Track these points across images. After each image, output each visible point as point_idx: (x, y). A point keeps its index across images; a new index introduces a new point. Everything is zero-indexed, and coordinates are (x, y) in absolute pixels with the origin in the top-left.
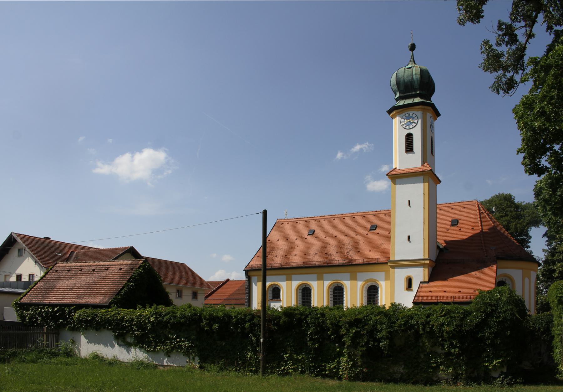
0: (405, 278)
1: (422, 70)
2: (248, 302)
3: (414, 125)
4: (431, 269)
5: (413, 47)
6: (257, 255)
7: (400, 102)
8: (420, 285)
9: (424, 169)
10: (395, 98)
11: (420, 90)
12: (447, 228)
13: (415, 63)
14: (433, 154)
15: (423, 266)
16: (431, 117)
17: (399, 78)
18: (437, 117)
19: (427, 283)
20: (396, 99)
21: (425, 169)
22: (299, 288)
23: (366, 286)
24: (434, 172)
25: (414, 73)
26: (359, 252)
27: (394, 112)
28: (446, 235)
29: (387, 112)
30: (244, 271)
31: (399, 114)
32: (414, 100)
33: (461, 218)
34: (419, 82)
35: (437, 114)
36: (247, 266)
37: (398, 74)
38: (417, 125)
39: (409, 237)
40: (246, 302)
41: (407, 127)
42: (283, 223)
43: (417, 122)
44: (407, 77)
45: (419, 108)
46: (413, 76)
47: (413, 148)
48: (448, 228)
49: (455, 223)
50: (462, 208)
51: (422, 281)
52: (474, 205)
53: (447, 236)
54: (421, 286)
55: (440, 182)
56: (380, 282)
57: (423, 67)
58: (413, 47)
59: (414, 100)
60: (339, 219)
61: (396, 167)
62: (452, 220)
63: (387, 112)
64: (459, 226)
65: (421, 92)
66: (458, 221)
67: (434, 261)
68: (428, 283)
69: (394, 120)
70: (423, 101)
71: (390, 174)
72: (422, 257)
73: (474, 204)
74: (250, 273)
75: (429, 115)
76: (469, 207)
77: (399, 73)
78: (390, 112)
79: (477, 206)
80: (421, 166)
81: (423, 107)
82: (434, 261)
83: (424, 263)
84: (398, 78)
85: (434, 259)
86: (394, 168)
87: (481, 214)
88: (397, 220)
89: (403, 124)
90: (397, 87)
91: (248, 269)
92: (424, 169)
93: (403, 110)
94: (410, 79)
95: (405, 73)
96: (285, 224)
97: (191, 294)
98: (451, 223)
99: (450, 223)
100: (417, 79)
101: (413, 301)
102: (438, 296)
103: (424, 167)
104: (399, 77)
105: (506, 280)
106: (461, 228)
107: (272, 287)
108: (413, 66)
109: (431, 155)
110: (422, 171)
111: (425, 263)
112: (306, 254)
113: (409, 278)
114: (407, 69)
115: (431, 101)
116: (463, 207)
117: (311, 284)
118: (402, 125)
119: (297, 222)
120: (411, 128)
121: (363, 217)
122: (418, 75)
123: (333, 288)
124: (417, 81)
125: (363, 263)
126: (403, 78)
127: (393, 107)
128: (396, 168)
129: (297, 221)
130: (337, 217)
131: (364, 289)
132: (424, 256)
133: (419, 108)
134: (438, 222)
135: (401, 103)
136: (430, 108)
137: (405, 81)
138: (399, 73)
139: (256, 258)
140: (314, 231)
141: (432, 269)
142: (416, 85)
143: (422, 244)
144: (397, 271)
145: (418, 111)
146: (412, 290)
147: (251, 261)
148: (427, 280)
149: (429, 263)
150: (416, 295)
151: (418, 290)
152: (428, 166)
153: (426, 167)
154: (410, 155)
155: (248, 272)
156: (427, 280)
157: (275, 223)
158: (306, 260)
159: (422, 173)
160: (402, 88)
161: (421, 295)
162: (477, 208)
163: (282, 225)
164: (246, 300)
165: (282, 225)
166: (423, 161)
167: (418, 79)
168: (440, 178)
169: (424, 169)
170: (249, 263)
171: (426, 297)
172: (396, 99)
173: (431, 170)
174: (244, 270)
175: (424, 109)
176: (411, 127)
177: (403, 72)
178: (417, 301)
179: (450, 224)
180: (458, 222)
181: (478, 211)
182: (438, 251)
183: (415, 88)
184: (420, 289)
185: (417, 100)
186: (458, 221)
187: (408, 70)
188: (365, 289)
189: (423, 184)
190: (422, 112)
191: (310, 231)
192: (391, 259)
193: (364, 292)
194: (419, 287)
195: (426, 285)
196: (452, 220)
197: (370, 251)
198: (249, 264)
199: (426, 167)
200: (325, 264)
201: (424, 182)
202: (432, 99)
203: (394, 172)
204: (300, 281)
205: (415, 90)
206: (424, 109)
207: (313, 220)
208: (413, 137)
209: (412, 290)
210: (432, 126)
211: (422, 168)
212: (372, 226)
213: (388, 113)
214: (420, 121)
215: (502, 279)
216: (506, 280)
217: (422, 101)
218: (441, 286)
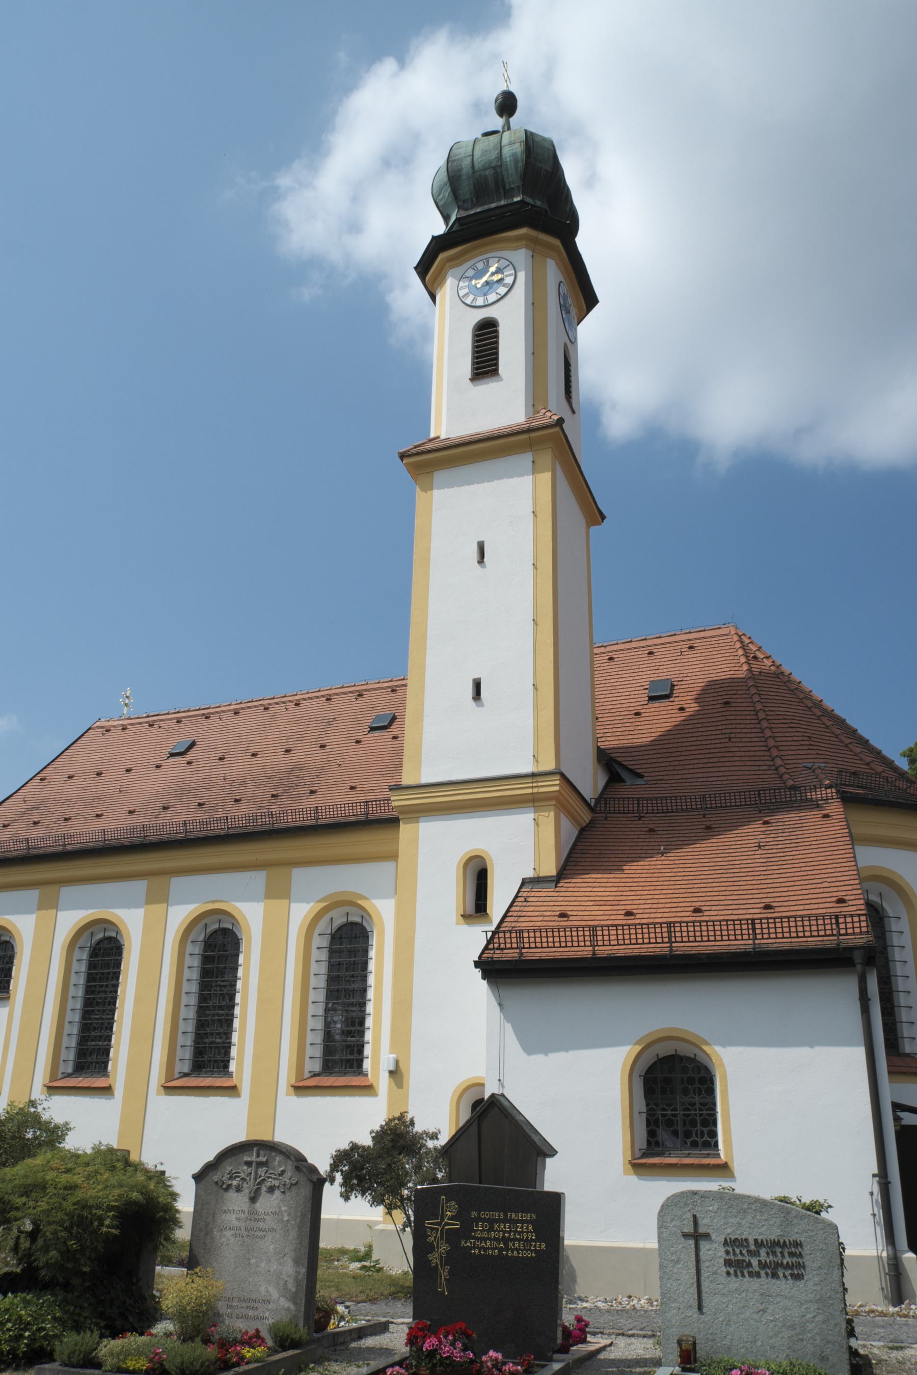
0: (458, 865)
3: (502, 290)
8: (519, 891)
11: (523, 193)
15: (533, 801)
16: (561, 282)
17: (458, 159)
19: (553, 884)
23: (323, 926)
26: (312, 792)
28: (631, 728)
34: (520, 164)
38: (513, 292)
39: (477, 685)
44: (482, 155)
45: (518, 239)
46: (501, 150)
47: (497, 364)
51: (530, 874)
52: (726, 637)
53: (636, 732)
54: (525, 894)
56: (374, 901)
61: (437, 435)
66: (673, 686)
68: (558, 882)
76: (708, 643)
83: (535, 790)
84: (454, 161)
86: (432, 435)
88: (431, 622)
89: (467, 294)
90: (449, 189)
94: (493, 158)
100: (514, 155)
101: (480, 957)
106: (685, 706)
111: (542, 790)
117: (122, 921)
118: (463, 296)
120: (490, 301)
122: (517, 145)
124: (516, 161)
125: (313, 822)
126: (469, 159)
132: (537, 761)
134: (598, 686)
137: (477, 167)
141: (576, 833)
142: (513, 177)
143: (529, 712)
145: (516, 248)
148: (550, 869)
149: (557, 788)
151: (508, 911)
154: (488, 387)
159: (526, 436)
160: (466, 189)
165: (103, 734)
166: (533, 405)
167: (519, 155)
176: (492, 298)
177: (472, 144)
178: (497, 955)
183: (507, 187)
184: (517, 909)
186: (673, 686)
189: (529, 479)
190: (530, 253)
192: (406, 780)
193: (316, 955)
194: (514, 901)
195: (548, 891)
201: (535, 471)
204: (87, 908)
208: (497, 332)
214: (521, 276)
218: (612, 894)
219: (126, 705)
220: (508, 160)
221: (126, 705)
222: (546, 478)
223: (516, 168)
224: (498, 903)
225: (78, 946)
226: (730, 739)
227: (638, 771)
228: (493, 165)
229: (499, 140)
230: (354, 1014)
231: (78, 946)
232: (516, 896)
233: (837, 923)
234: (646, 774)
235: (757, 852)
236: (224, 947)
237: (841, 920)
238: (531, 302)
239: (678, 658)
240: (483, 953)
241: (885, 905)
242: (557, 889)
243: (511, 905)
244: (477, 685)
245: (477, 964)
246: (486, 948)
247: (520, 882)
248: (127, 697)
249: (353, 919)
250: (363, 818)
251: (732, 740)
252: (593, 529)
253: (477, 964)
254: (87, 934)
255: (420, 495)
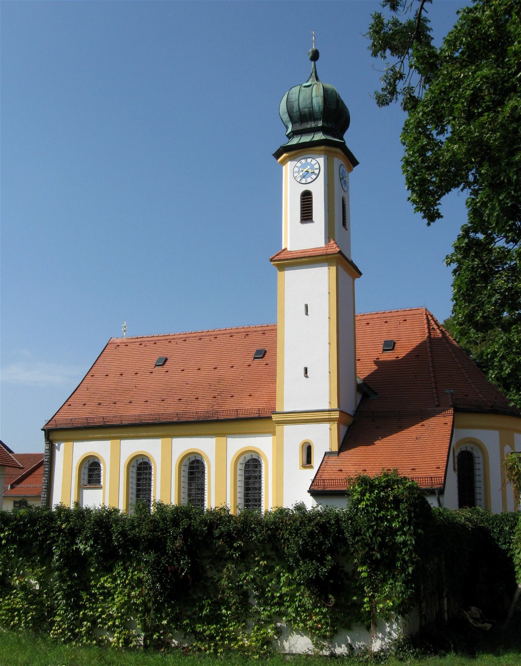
1: (325, 90)
2: (46, 490)
3: (314, 177)
4: (344, 429)
5: (315, 56)
6: (68, 403)
7: (293, 139)
8: (324, 458)
9: (328, 251)
10: (287, 134)
12: (377, 355)
13: (317, 79)
14: (347, 228)
18: (354, 167)
19: (337, 455)
20: (287, 136)
21: (330, 250)
22: (184, 463)
24: (346, 255)
25: (314, 94)
27: (285, 155)
29: (273, 155)
30: (43, 432)
31: (291, 158)
32: (313, 137)
33: (399, 337)
34: (321, 108)
35: (354, 162)
36: (50, 421)
37: (290, 96)
39: (306, 370)
40: (44, 490)
41: (303, 181)
42: (118, 346)
43: (318, 173)
45: (321, 151)
47: (312, 215)
48: (379, 355)
49: (391, 347)
50: (401, 321)
51: (328, 450)
55: (360, 274)
57: (329, 86)
58: (315, 56)
59: (313, 137)
60: (208, 338)
61: (286, 247)
62: (385, 342)
63: (273, 155)
64: (396, 351)
65: (325, 124)
67: (352, 414)
69: (284, 167)
70: (326, 139)
71: (277, 258)
72: (327, 407)
73: (420, 314)
74: (53, 436)
75: (337, 162)
77: (292, 94)
78: (277, 155)
79: (425, 317)
80: (324, 246)
81: (328, 148)
82: (352, 414)
84: (290, 102)
85: (351, 409)
86: (283, 248)
87: (431, 331)
91: (49, 427)
92: (328, 251)
93: (298, 153)
95: (300, 95)
96: (122, 348)
97: (477, 468)
98: (384, 347)
99: (381, 347)
101: (310, 489)
102: (432, 478)
103: (329, 248)
104: (291, 100)
105: (472, 448)
107: (89, 461)
108: (313, 84)
109: (343, 229)
110: (326, 255)
111: (332, 417)
112: (147, 401)
113: (248, 457)
114: (303, 89)
115: (343, 140)
116: (404, 319)
119: (141, 344)
121: (246, 335)
122: (320, 97)
123: (188, 463)
127: (281, 147)
128: (286, 249)
129: (141, 342)
130: (205, 336)
131: (239, 466)
133: (321, 151)
135: (295, 141)
136: (339, 150)
138: (292, 94)
139: (66, 407)
140: (166, 360)
144: (288, 429)
146: (312, 467)
147: (57, 413)
148: (336, 449)
149: (338, 416)
150: (315, 477)
151: (320, 468)
152: (335, 246)
153: (332, 248)
154: (308, 226)
155: (50, 434)
156: (337, 450)
157: (106, 346)
158: (147, 412)
159: (325, 257)
161: (323, 477)
162: (425, 321)
163: (116, 348)
164: (44, 487)
165: (116, 348)
168: (360, 268)
169: (330, 251)
170: (54, 416)
171: (435, 479)
172: (287, 136)
173: (340, 252)
174: (42, 430)
175: (329, 151)
176: (309, 180)
178: (316, 488)
179: (382, 348)
180: (394, 346)
181: (426, 326)
182: (359, 397)
183: (315, 117)
185: (319, 136)
186: (394, 343)
187: (306, 90)
188: (241, 467)
190: (326, 157)
191: (160, 359)
192: (278, 410)
194: (322, 463)
195: (334, 458)
196: (385, 342)
197: (249, 396)
198: (52, 418)
199: (332, 248)
200: (175, 420)
202: (346, 136)
203: (282, 256)
205: (315, 120)
206: (329, 151)
207: (167, 340)
208: (311, 198)
209: (312, 467)
210: (344, 181)
211: (326, 248)
212: (258, 352)
213: (275, 157)
215: (466, 447)
216: (472, 448)
217: (325, 138)
219: (125, 331)
220: (315, 105)
221: (125, 331)
222: (334, 269)
223: (319, 109)
224: (317, 459)
225: (131, 465)
226: (416, 376)
227: (376, 391)
228: (309, 106)
229: (310, 92)
230: (256, 498)
231: (131, 465)
232: (323, 461)
233: (432, 480)
234: (379, 393)
235: (416, 441)
236: (197, 468)
237: (433, 479)
238: (327, 183)
239: (398, 326)
240: (311, 487)
241: (474, 452)
242: (338, 457)
243: (321, 465)
244: (306, 370)
245: (308, 492)
246: (312, 485)
247: (324, 453)
248: (125, 327)
249: (254, 457)
250: (257, 415)
251: (418, 377)
252: (357, 280)
253: (308, 492)
254: (135, 460)
255: (280, 274)
